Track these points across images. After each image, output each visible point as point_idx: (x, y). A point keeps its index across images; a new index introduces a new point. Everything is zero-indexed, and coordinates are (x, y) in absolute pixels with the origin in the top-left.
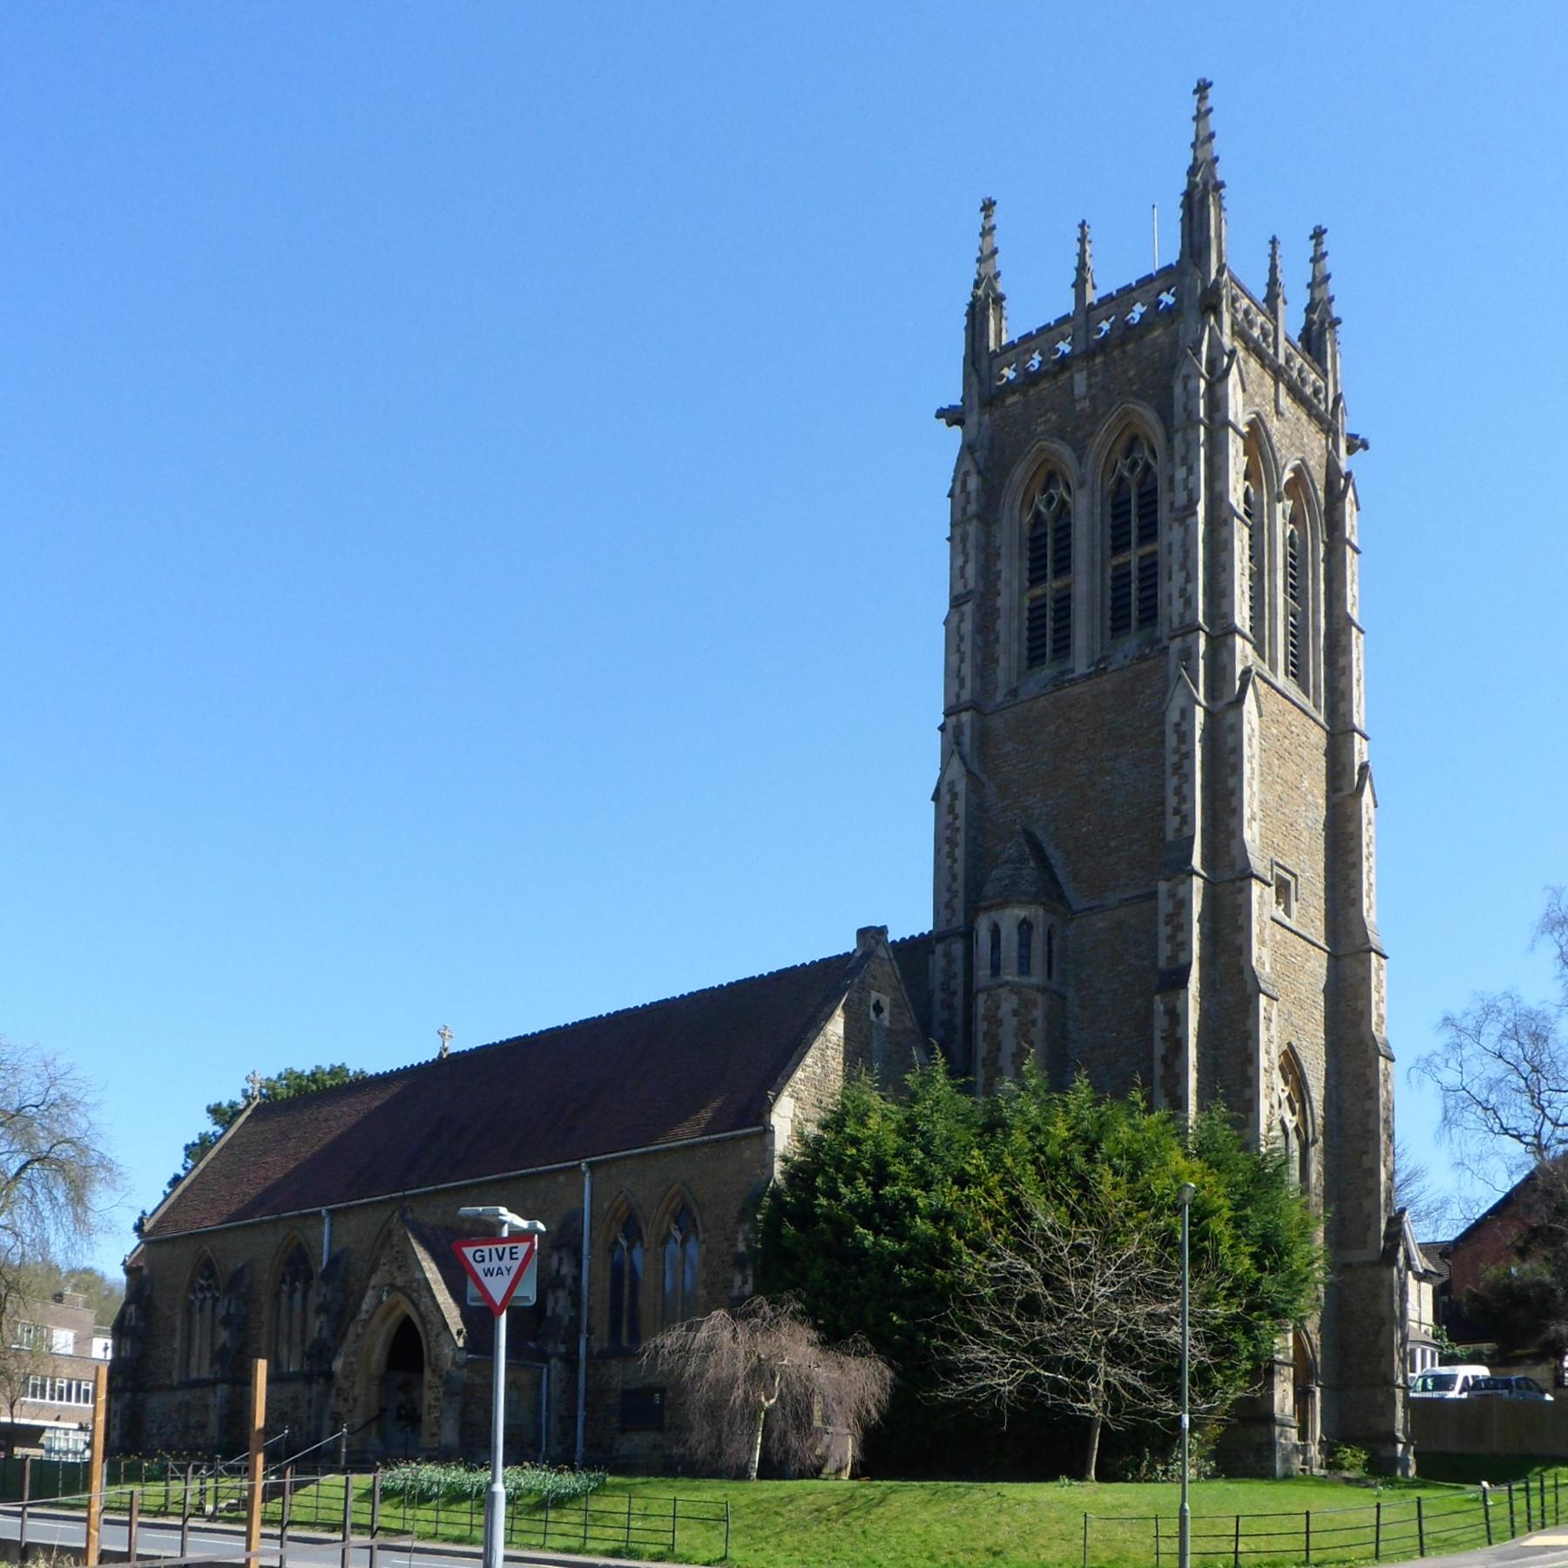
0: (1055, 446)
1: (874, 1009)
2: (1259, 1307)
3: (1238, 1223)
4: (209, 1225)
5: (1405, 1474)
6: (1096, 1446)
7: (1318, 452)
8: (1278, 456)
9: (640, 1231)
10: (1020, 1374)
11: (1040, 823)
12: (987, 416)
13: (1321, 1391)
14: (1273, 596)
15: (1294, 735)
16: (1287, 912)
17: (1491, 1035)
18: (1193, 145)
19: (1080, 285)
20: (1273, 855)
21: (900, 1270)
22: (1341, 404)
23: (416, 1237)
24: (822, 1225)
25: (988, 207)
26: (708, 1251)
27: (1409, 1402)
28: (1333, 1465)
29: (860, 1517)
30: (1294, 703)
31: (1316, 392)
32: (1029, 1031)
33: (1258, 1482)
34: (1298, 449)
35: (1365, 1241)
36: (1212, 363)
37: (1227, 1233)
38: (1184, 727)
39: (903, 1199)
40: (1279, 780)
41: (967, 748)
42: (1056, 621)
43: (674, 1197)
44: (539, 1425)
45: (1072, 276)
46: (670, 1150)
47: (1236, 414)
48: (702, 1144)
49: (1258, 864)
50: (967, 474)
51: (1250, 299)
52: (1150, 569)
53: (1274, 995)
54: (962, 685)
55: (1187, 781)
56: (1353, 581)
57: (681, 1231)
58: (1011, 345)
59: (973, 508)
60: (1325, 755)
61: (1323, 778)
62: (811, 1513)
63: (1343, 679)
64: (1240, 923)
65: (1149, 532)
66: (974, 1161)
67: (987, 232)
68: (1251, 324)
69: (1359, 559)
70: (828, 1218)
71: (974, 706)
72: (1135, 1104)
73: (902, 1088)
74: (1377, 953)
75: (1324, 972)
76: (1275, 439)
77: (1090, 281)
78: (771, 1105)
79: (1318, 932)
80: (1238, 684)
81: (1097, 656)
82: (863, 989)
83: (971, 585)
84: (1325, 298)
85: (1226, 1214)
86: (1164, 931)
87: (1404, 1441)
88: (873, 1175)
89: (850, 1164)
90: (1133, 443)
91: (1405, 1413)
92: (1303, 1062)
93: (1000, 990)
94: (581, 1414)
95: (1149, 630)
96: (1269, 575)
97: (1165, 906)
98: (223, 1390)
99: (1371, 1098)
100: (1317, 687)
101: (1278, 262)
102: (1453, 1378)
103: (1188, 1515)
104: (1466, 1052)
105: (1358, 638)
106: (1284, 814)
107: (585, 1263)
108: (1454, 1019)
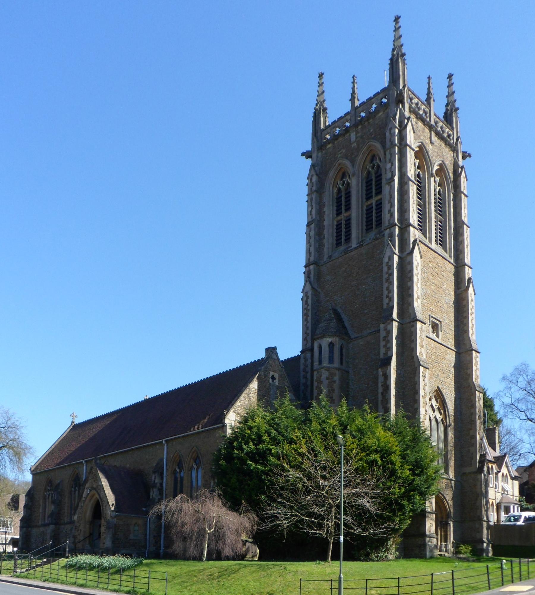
0: (344, 162)
1: (271, 379)
2: (414, 490)
3: (403, 457)
4: (50, 468)
5: (487, 555)
7: (450, 159)
8: (431, 159)
10: (294, 519)
11: (340, 306)
12: (320, 153)
13: (453, 523)
14: (430, 213)
15: (440, 267)
16: (437, 336)
17: (522, 383)
18: (394, 41)
19: (352, 100)
20: (430, 313)
21: (265, 478)
22: (459, 140)
24: (236, 461)
25: (321, 76)
26: (205, 473)
27: (489, 527)
28: (457, 552)
31: (449, 136)
32: (333, 385)
34: (440, 157)
35: (471, 464)
36: (401, 123)
37: (398, 460)
39: (267, 449)
40: (433, 284)
42: (346, 229)
43: (194, 452)
44: (146, 539)
45: (350, 97)
46: (192, 434)
47: (411, 142)
48: (202, 431)
49: (419, 316)
50: (312, 176)
51: (418, 99)
52: (379, 206)
53: (427, 367)
54: (310, 256)
55: (391, 285)
56: (465, 208)
58: (329, 126)
60: (454, 275)
61: (453, 284)
62: (208, 576)
63: (461, 246)
65: (379, 191)
66: (296, 434)
67: (320, 85)
68: (419, 109)
69: (467, 199)
70: (239, 458)
71: (315, 263)
72: (366, 410)
73: (272, 406)
74: (475, 351)
75: (454, 359)
76: (430, 153)
77: (356, 98)
78: (225, 415)
80: (411, 245)
81: (360, 240)
83: (314, 217)
84: (453, 100)
85: (398, 453)
86: (382, 343)
88: (256, 441)
89: (248, 437)
90: (373, 157)
92: (444, 394)
93: (322, 370)
95: (379, 229)
96: (428, 206)
97: (383, 334)
98: (52, 527)
99: (473, 408)
100: (450, 249)
101: (431, 85)
102: (520, 517)
103: (342, 579)
104: (513, 390)
105: (467, 229)
106: (435, 297)
107: (164, 478)
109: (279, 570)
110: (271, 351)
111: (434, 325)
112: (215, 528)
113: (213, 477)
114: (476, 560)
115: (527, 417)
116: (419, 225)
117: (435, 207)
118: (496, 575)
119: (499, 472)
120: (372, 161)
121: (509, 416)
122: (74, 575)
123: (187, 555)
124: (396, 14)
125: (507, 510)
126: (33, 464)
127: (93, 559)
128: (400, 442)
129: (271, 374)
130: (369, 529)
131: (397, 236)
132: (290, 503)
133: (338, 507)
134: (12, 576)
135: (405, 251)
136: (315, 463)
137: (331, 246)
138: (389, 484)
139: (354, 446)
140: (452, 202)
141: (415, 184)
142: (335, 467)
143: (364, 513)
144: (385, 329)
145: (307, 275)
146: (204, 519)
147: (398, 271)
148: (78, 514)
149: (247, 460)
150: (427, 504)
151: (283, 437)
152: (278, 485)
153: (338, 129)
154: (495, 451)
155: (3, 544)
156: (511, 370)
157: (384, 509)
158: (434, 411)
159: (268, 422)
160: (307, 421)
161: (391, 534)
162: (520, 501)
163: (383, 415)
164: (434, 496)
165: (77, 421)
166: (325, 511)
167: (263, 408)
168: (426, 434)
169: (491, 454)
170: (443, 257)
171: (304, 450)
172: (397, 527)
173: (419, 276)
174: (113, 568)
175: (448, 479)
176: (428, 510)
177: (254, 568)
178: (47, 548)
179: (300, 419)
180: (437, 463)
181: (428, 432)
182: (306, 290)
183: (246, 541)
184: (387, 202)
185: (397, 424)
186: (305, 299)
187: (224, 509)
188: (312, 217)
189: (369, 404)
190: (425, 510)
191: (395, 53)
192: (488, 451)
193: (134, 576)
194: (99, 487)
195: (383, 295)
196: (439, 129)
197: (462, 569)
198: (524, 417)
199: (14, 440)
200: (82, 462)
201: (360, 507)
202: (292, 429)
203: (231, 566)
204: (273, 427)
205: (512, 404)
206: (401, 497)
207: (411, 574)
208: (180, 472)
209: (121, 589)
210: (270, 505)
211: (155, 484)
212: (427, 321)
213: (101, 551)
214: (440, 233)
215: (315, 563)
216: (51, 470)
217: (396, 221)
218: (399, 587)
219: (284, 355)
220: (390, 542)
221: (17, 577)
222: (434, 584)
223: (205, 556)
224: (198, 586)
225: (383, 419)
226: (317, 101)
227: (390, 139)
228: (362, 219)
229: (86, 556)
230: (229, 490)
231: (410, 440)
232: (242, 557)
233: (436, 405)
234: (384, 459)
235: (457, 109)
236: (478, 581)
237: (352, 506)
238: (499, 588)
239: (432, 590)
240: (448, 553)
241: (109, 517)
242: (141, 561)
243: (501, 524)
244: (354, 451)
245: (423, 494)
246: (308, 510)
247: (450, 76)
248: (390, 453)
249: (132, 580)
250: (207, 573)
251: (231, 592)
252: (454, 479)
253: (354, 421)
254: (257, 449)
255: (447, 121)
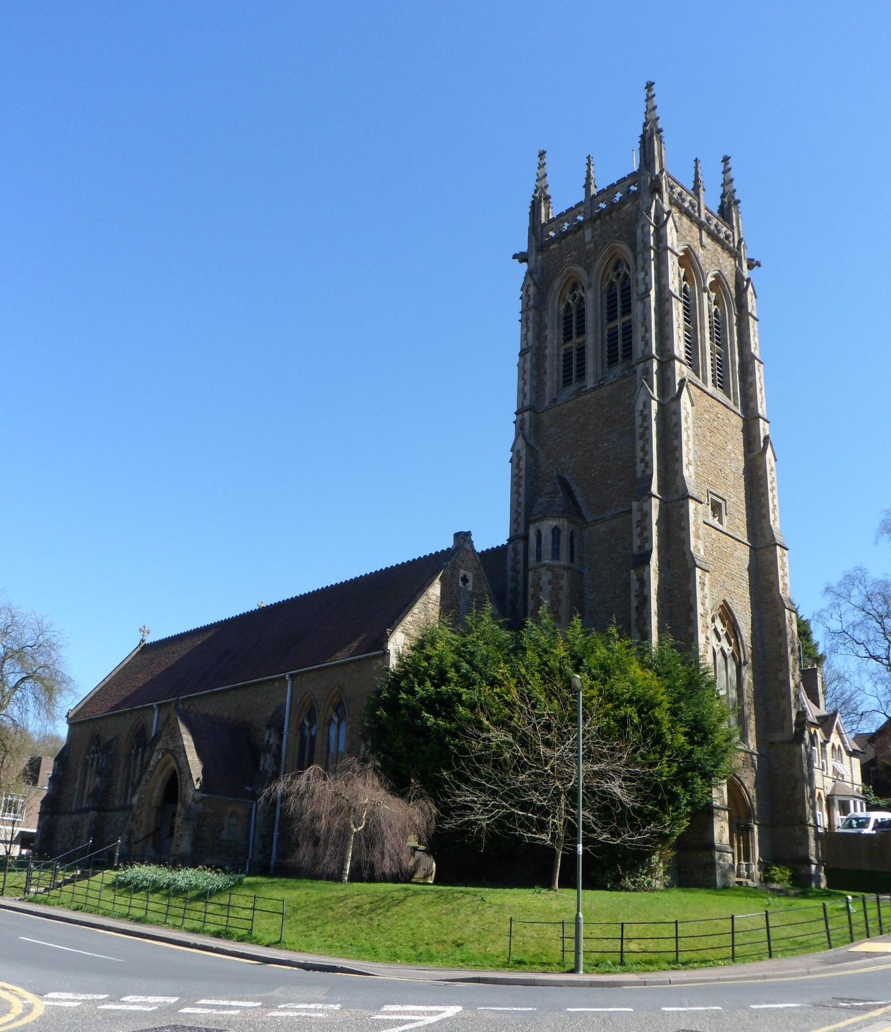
1: (462, 580)
2: (693, 770)
3: (674, 712)
4: (100, 714)
5: (818, 887)
6: (559, 865)
7: (730, 268)
8: (703, 268)
9: (315, 718)
12: (540, 257)
13: (758, 828)
15: (720, 420)
17: (857, 596)
18: (646, 113)
19: (587, 186)
21: (450, 741)
22: (743, 243)
23: (182, 720)
24: (403, 711)
25: (542, 154)
26: (351, 729)
27: (818, 836)
28: (767, 879)
29: (381, 914)
30: (719, 401)
31: (727, 237)
32: (558, 593)
33: (703, 891)
34: (716, 265)
35: (783, 728)
36: (658, 218)
37: (667, 718)
38: (645, 413)
39: (453, 694)
41: (527, 431)
42: (578, 360)
44: (248, 840)
46: (334, 665)
47: (672, 244)
48: (351, 662)
49: (692, 490)
50: (528, 286)
52: (628, 329)
53: (706, 568)
56: (754, 336)
57: (338, 716)
59: (531, 303)
62: (352, 909)
63: (751, 389)
64: (682, 526)
65: (627, 309)
67: (541, 166)
68: (683, 200)
70: (407, 707)
71: (531, 408)
74: (781, 546)
75: (748, 558)
76: (701, 260)
78: (388, 637)
79: (742, 533)
80: (677, 387)
81: (599, 378)
82: (454, 568)
83: (530, 343)
84: (731, 190)
85: (666, 705)
86: (636, 531)
87: (816, 862)
91: (817, 844)
92: (735, 613)
93: (541, 569)
94: (276, 834)
95: (628, 362)
97: (636, 516)
99: (782, 635)
100: (735, 394)
101: (699, 170)
102: (868, 820)
103: (582, 922)
104: (843, 609)
105: (758, 366)
107: (285, 736)
108: (832, 588)
109: (473, 901)
110: (463, 538)
111: (714, 504)
112: (366, 825)
113: (364, 737)
114: (800, 893)
115: (869, 652)
116: (687, 358)
117: (710, 333)
118: (838, 922)
119: (826, 742)
120: (616, 268)
121: (839, 651)
122: (126, 901)
123: (319, 869)
124: (648, 79)
125: (844, 808)
126: (72, 708)
127: (160, 872)
128: (668, 687)
129: (462, 572)
130: (622, 834)
131: (656, 373)
132: (491, 784)
133: (572, 794)
134: (20, 900)
135: (669, 395)
136: (534, 719)
137: (555, 385)
138: (652, 757)
139: (595, 692)
140: (735, 328)
141: (681, 301)
142: (566, 727)
143: (614, 806)
144: (640, 509)
145: (520, 426)
146: (350, 808)
147: (657, 424)
148: (140, 794)
149: (421, 710)
150: (715, 794)
151: (481, 675)
152: (473, 754)
153: (566, 224)
154: (819, 707)
155: (5, 842)
156: (840, 578)
157: (645, 799)
158: (719, 640)
159: (457, 649)
160: (518, 649)
161: (658, 843)
162: (864, 793)
163: (638, 644)
164: (725, 781)
165: (149, 640)
166: (549, 800)
167: (448, 626)
168: (709, 676)
169: (813, 713)
170: (725, 405)
171: (514, 695)
172: (667, 831)
173: (690, 432)
174: (192, 889)
175: (746, 752)
176: (717, 803)
177: (430, 897)
178: (84, 852)
179: (506, 647)
180: (730, 724)
181: (712, 674)
182: (518, 447)
183: (415, 849)
184: (639, 325)
185: (662, 659)
186: (516, 460)
187: (382, 792)
188: (527, 344)
189: (617, 625)
190: (712, 803)
191: (647, 128)
192: (807, 706)
193: (229, 906)
194: (178, 749)
195: (635, 458)
196: (712, 228)
197: (780, 909)
198: (863, 653)
199: (46, 666)
200: (152, 706)
201: (606, 795)
202: (495, 662)
203: (390, 892)
204: (463, 657)
205: (844, 631)
206: (672, 780)
207: (696, 916)
208: (310, 727)
209: (206, 928)
210: (458, 788)
211: (267, 749)
212: (704, 499)
213: (172, 859)
214: (719, 370)
215: (532, 890)
216: (100, 718)
217: (654, 352)
218: (677, 937)
219: (481, 544)
220: (655, 858)
221: (30, 901)
222: (736, 935)
223: (348, 872)
224: (336, 927)
225: (639, 650)
226: (537, 186)
227: (643, 240)
228: (602, 346)
229: (148, 867)
230: (390, 759)
231: (684, 685)
232: (403, 876)
233: (722, 630)
234: (643, 715)
235: (737, 202)
236: (808, 932)
237: (594, 794)
238: (847, 946)
239: (733, 946)
240: (753, 881)
241: (189, 801)
242: (240, 880)
243: (837, 831)
244: (594, 701)
245: (707, 776)
246: (523, 797)
247: (726, 160)
248: (653, 705)
249: (225, 912)
250: (350, 903)
251: (392, 939)
252: (756, 752)
253: (593, 652)
254: (438, 693)
255: (723, 218)
